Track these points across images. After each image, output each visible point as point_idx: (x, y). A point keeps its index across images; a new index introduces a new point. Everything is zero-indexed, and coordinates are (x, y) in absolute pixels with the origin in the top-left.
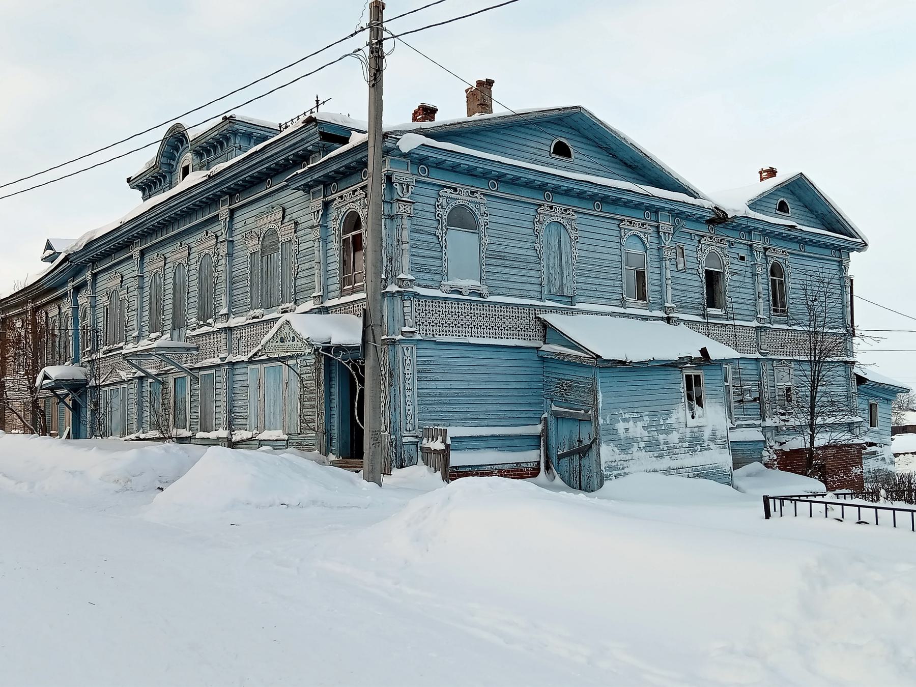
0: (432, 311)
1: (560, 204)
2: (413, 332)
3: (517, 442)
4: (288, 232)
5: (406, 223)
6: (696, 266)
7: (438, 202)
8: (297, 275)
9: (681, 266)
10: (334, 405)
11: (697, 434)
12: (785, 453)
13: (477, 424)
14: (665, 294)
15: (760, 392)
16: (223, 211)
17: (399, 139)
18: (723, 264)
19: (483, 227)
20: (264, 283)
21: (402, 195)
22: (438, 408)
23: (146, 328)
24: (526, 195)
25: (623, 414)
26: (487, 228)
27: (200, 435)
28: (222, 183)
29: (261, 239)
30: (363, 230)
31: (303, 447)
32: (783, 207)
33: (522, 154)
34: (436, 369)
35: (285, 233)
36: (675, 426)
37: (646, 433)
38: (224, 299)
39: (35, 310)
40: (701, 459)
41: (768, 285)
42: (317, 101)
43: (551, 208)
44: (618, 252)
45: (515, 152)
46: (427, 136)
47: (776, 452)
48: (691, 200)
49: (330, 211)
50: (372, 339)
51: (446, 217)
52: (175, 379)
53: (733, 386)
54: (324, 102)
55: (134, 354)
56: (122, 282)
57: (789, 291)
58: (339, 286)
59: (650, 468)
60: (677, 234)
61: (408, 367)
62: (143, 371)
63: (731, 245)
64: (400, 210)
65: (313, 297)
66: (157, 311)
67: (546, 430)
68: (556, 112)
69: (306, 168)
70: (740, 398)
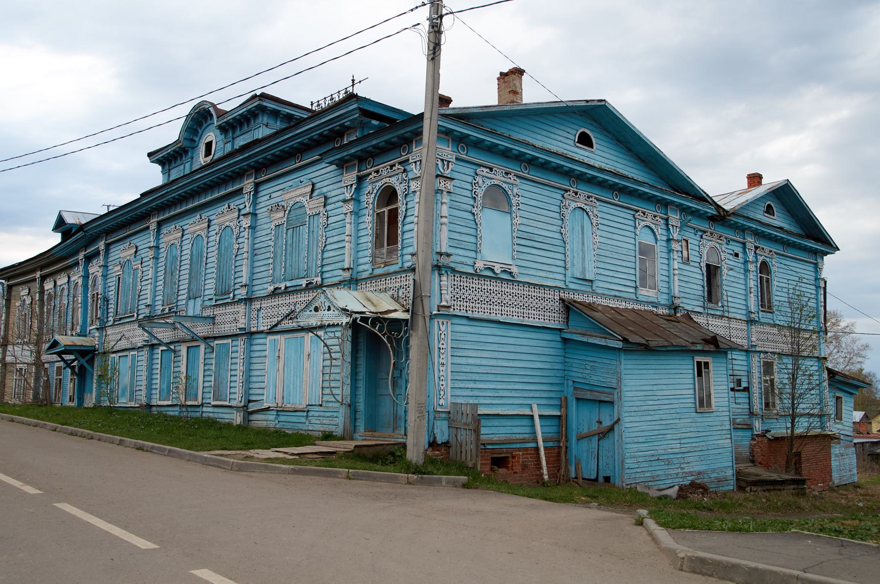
1: (584, 191)
7: (475, 180)
8: (324, 247)
14: (672, 284)
16: (248, 184)
20: (288, 256)
29: (287, 212)
30: (399, 204)
42: (353, 80)
43: (576, 194)
44: (632, 241)
51: (482, 195)
54: (360, 82)
56: (136, 252)
57: (774, 288)
64: (441, 185)
68: (583, 104)
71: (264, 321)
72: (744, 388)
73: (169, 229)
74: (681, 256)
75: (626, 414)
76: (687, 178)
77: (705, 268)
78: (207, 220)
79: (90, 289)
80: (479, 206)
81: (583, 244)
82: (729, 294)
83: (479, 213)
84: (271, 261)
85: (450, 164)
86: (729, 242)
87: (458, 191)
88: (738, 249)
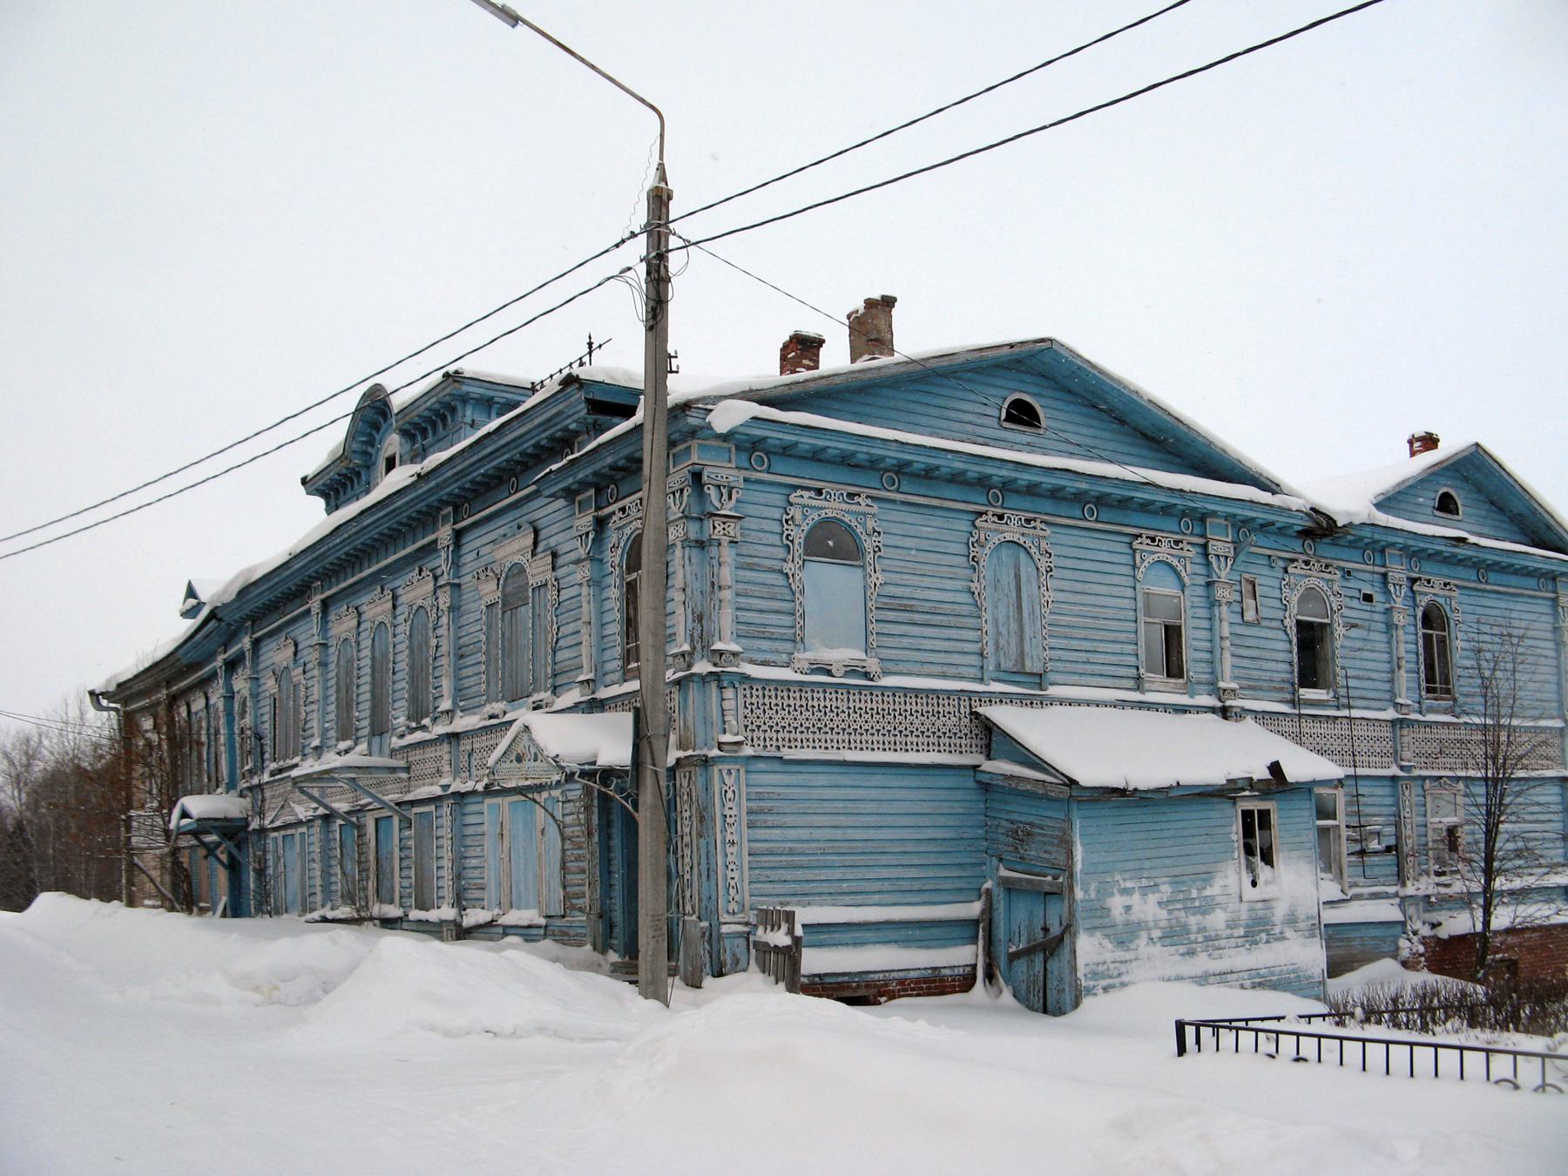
0: (777, 705)
2: (739, 744)
3: (934, 932)
4: (542, 569)
5: (728, 553)
6: (1280, 614)
8: (556, 643)
9: (1250, 615)
10: (614, 868)
11: (1261, 913)
12: (1439, 941)
13: (860, 902)
15: (1398, 837)
16: (444, 533)
17: (711, 410)
18: (1332, 609)
19: (872, 555)
21: (719, 506)
22: (789, 875)
23: (332, 733)
24: (956, 499)
25: (1121, 882)
26: (879, 556)
27: (415, 914)
28: (439, 487)
29: (501, 582)
31: (565, 937)
32: (1446, 505)
33: (945, 424)
34: (786, 807)
35: (539, 570)
36: (1219, 899)
37: (1163, 914)
38: (447, 685)
39: (173, 699)
40: (1266, 956)
41: (1417, 644)
42: (590, 344)
44: (1129, 593)
45: (933, 422)
46: (762, 402)
47: (1424, 940)
48: (1265, 497)
49: (606, 534)
50: (649, 760)
51: (802, 540)
52: (376, 819)
53: (1347, 826)
54: (600, 346)
55: (308, 777)
56: (295, 654)
58: (620, 663)
59: (1170, 972)
60: (1242, 557)
61: (730, 804)
62: (326, 807)
63: (1348, 573)
64: (716, 531)
65: (581, 682)
66: (346, 705)
67: (989, 909)
68: (1007, 350)
69: (564, 462)
70: (1357, 847)
71: (478, 772)
79: (237, 718)
80: (797, 559)
82: (1350, 673)
83: (797, 571)
84: (483, 667)
85: (734, 491)
87: (753, 536)
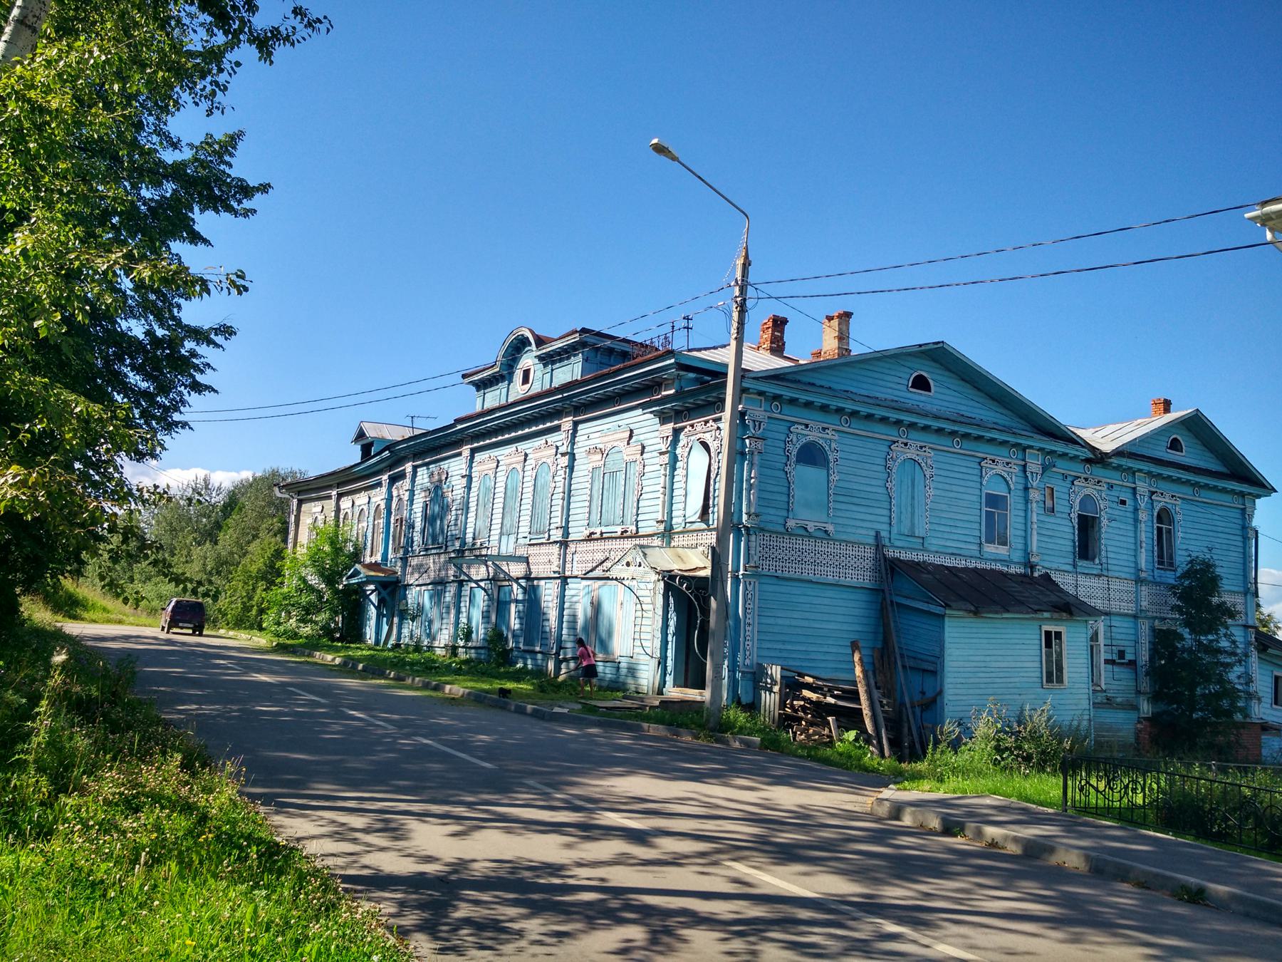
16: (566, 423)
29: (605, 455)
43: (906, 444)
72: (1130, 661)
73: (483, 457)
74: (1043, 506)
75: (950, 686)
76: (1050, 419)
77: (1077, 520)
78: (523, 454)
79: (393, 513)
81: (913, 498)
86: (1112, 487)
88: (1126, 496)
